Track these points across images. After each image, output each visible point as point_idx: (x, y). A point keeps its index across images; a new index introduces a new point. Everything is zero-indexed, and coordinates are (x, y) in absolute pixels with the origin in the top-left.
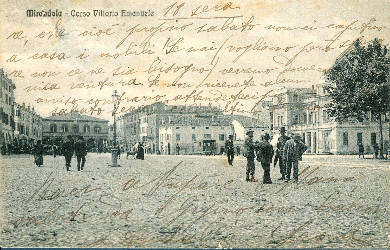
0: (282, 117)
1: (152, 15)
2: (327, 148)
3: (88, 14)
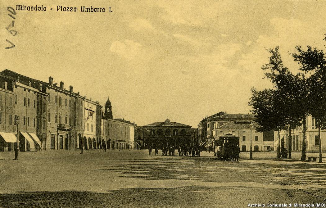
3: (104, 10)
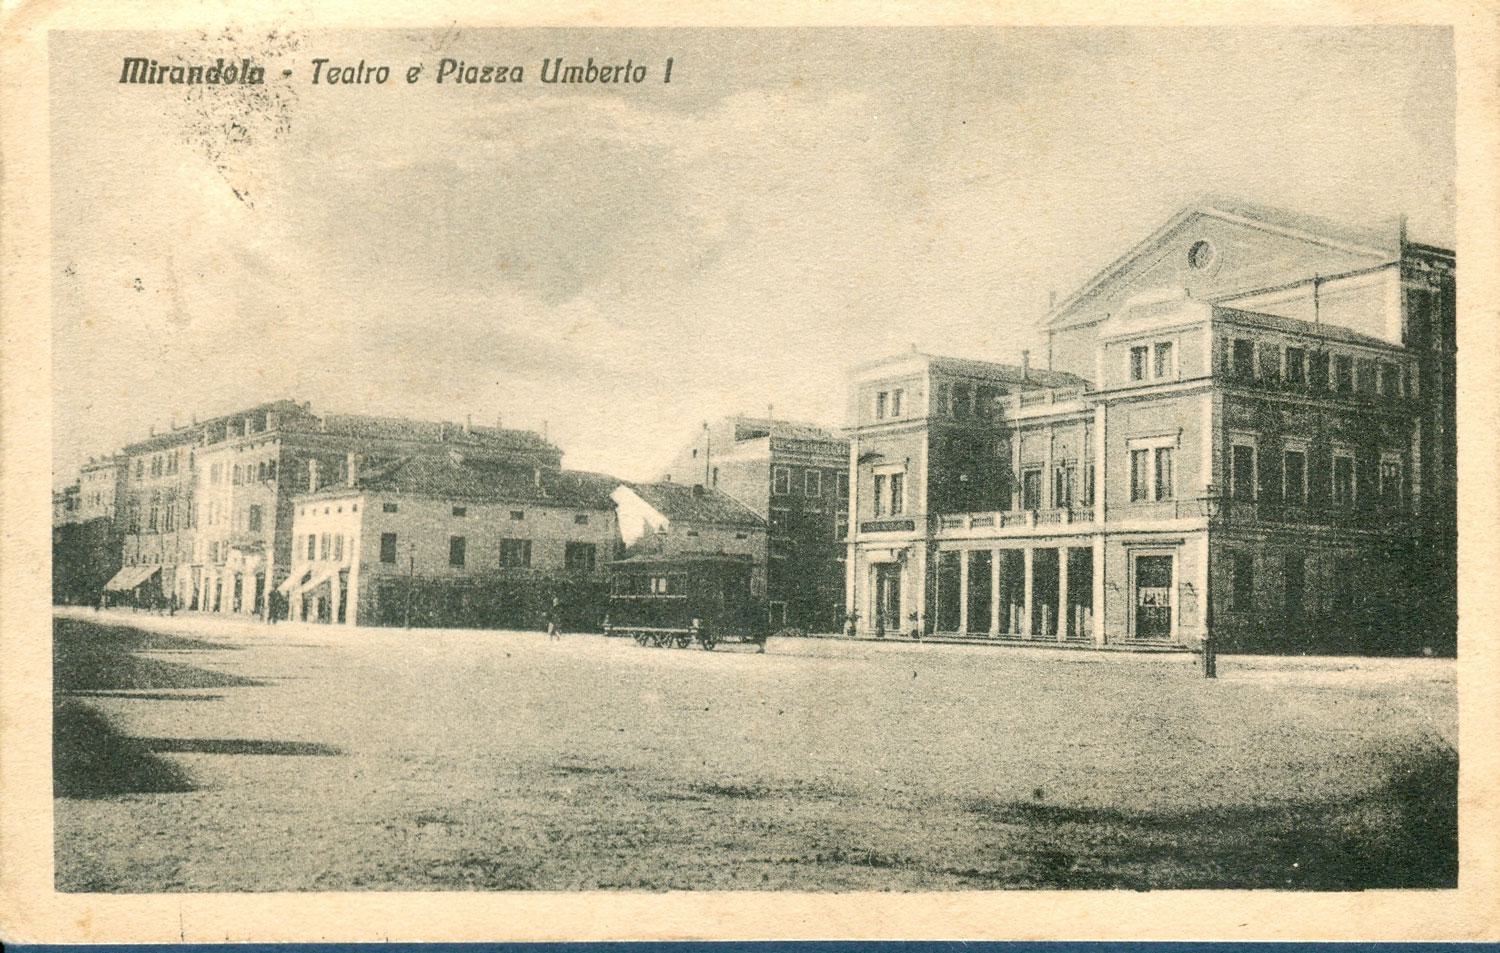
0: (895, 477)
1: (605, 78)
2: (1150, 624)
